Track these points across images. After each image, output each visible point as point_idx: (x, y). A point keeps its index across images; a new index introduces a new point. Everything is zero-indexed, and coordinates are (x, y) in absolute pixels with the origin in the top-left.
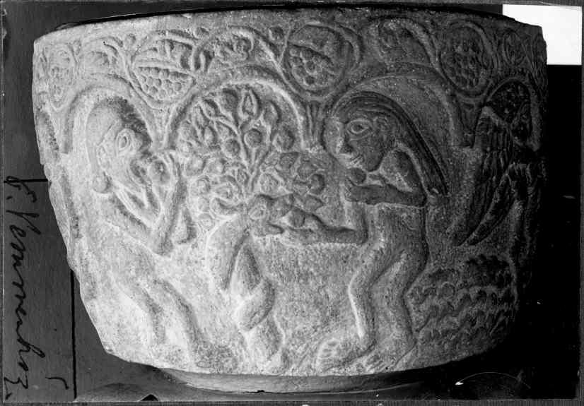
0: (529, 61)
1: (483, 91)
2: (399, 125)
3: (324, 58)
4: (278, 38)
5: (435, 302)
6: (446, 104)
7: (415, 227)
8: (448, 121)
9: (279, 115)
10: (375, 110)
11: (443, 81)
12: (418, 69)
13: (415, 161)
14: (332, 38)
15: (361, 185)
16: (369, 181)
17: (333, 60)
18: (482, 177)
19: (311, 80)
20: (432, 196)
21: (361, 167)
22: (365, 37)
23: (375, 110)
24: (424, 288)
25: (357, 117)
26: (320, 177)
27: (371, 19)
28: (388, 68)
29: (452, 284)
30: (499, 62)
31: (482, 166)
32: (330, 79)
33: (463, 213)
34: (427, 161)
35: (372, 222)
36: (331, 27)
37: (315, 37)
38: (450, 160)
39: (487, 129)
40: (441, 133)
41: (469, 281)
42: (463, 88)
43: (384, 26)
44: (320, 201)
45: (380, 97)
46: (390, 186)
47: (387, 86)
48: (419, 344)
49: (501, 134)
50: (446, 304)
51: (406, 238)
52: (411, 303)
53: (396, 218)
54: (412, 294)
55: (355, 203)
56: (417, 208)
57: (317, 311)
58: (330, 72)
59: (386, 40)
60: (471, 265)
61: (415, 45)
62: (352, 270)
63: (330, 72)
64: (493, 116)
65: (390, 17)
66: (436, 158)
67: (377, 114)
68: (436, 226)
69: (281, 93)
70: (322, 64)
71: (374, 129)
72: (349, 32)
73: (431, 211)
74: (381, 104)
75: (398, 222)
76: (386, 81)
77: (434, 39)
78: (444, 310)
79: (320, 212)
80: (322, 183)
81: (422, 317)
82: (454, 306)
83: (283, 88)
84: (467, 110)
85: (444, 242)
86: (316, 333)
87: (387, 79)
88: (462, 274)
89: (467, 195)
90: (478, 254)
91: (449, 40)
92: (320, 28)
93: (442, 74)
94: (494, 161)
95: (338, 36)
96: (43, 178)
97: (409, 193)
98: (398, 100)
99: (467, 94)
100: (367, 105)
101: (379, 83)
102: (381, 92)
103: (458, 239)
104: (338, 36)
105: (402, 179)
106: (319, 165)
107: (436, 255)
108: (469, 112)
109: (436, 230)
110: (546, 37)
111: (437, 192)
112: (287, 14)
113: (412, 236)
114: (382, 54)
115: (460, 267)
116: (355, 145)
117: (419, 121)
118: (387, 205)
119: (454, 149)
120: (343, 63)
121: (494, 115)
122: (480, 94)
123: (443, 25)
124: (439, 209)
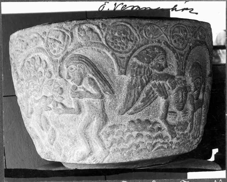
0: (165, 36)
1: (130, 51)
2: (88, 67)
3: (58, 42)
4: (45, 35)
5: (115, 137)
6: (111, 57)
7: (99, 107)
8: (113, 64)
9: (46, 65)
10: (77, 62)
11: (109, 48)
12: (95, 44)
13: (96, 81)
14: (61, 34)
15: (76, 91)
16: (79, 90)
17: (62, 43)
18: (131, 87)
19: (55, 52)
20: (106, 95)
21: (75, 84)
22: (74, 32)
23: (77, 62)
24: (108, 131)
25: (71, 65)
26: (61, 88)
27: (76, 25)
28: (82, 44)
29: (122, 130)
30: (141, 38)
31: (132, 82)
32: (61, 50)
33: (123, 101)
34: (102, 81)
35: (83, 105)
36: (61, 30)
37: (56, 34)
38: (115, 80)
39: (134, 67)
40: (110, 69)
41: (130, 129)
42: (119, 51)
43: (81, 27)
44: (62, 97)
45: (81, 56)
46: (87, 91)
47: (84, 52)
48: (111, 153)
49: (143, 69)
50: (120, 138)
51: (95, 111)
52: (103, 137)
53: (91, 104)
54: (102, 134)
55: (74, 98)
56: (100, 100)
57: (69, 139)
58: (61, 47)
59: (81, 33)
60: (131, 123)
61: (94, 34)
62: (78, 124)
63: (61, 47)
64: (138, 61)
65: (83, 24)
66: (108, 80)
67: (78, 63)
68: (110, 107)
69: (44, 57)
70: (58, 45)
71: (77, 69)
72: (67, 31)
73: (107, 101)
74: (82, 59)
75: (92, 105)
76: (84, 50)
77: (102, 30)
78: (119, 141)
79: (64, 102)
80: (62, 91)
81: (109, 143)
82: (124, 139)
83: (46, 55)
84: (121, 60)
85: (115, 113)
86: (71, 147)
87: (84, 49)
88: (126, 127)
89: (125, 94)
90: (136, 118)
91: (110, 31)
92: (57, 30)
93: (106, 45)
94: (139, 80)
95: (64, 33)
96: (14, 95)
97: (95, 94)
98: (89, 57)
99: (120, 53)
100: (74, 60)
101: (81, 51)
102: (82, 54)
103: (121, 113)
104: (64, 33)
105: (92, 88)
106: (61, 84)
107: (112, 119)
108: (122, 60)
109: (110, 108)
110: (211, 27)
111: (109, 93)
112: (48, 26)
113: (98, 111)
114: (80, 39)
115: (126, 124)
116: (71, 76)
117: (99, 65)
118: (87, 99)
119: (117, 75)
120: (65, 44)
121: (138, 61)
122: (128, 52)
123: (108, 25)
124: (111, 100)
